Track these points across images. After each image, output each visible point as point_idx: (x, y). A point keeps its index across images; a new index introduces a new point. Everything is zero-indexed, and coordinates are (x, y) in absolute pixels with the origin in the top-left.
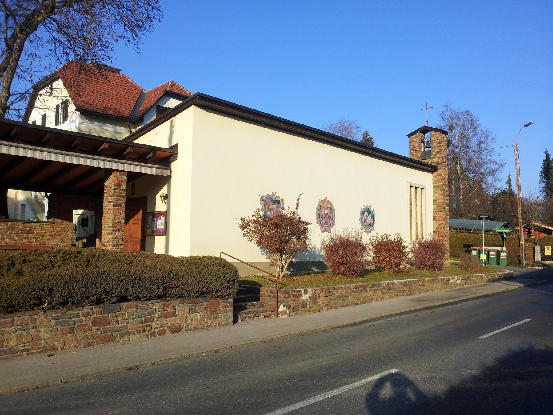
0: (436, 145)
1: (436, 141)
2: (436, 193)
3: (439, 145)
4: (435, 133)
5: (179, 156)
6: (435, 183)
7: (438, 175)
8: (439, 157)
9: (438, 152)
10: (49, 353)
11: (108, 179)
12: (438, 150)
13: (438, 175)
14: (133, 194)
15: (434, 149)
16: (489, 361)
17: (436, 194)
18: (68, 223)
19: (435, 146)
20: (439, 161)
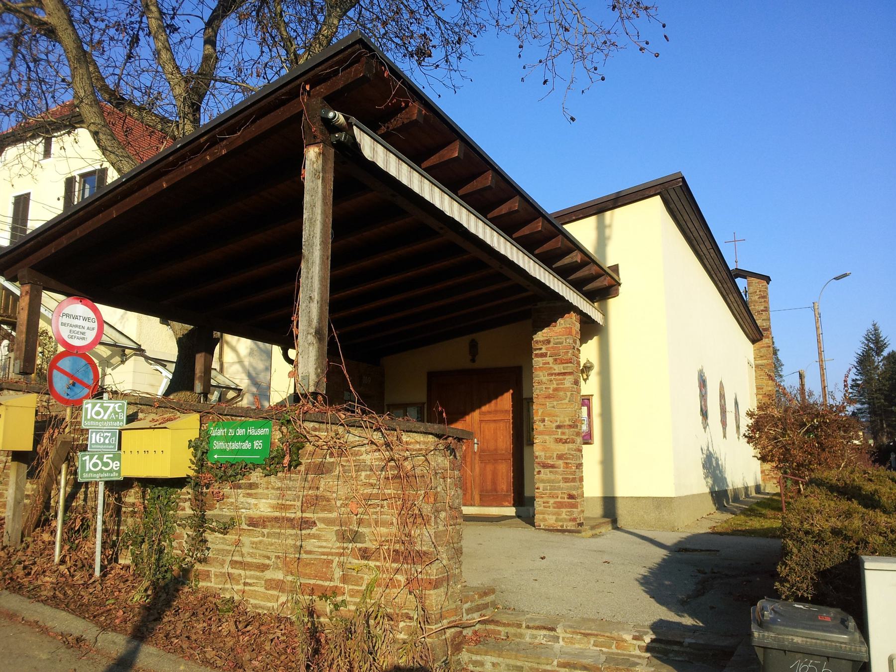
0: (757, 299)
1: (758, 293)
2: (760, 376)
3: (763, 300)
4: (754, 280)
5: (621, 289)
6: (758, 359)
7: (763, 347)
8: (763, 318)
9: (762, 311)
10: (606, 558)
11: (548, 326)
12: (762, 308)
13: (763, 347)
14: (473, 360)
15: (754, 306)
16: (316, 358)
17: (762, 377)
18: (188, 393)
19: (756, 302)
20: (765, 324)
